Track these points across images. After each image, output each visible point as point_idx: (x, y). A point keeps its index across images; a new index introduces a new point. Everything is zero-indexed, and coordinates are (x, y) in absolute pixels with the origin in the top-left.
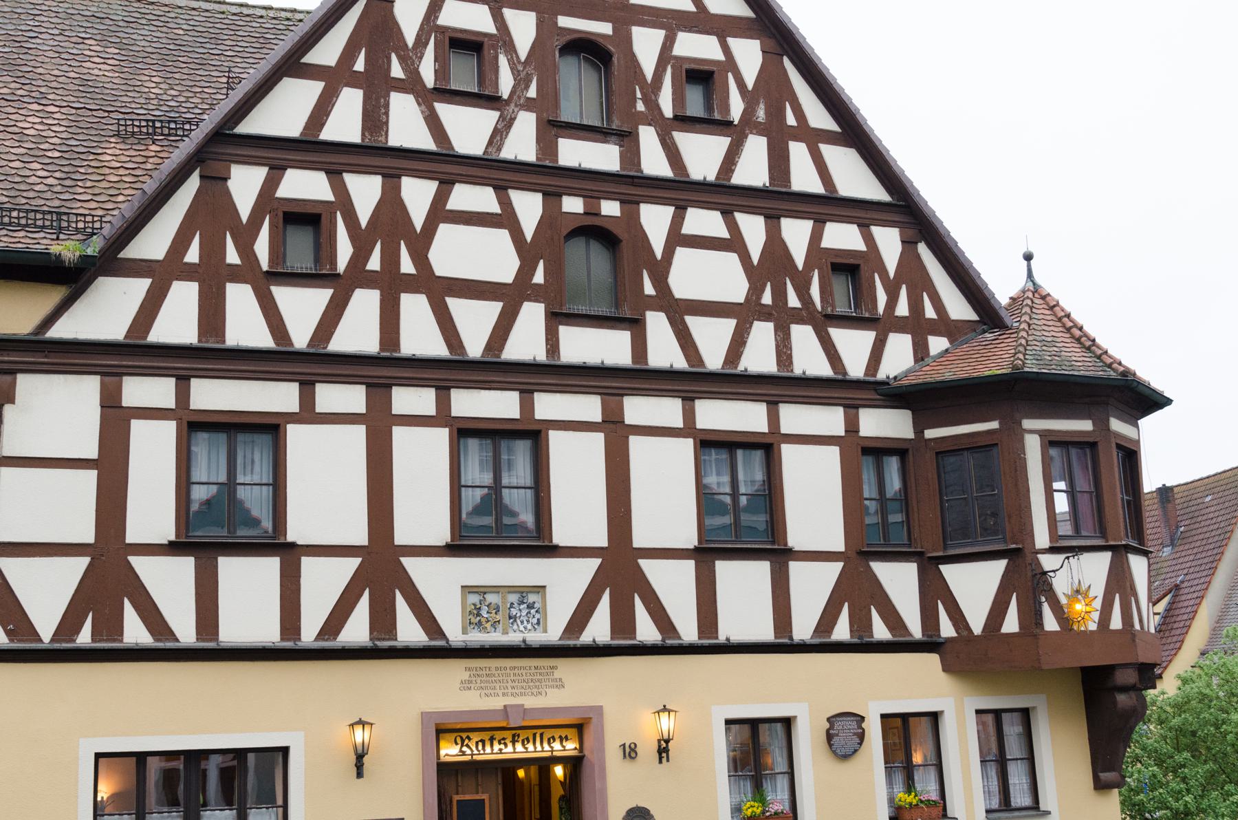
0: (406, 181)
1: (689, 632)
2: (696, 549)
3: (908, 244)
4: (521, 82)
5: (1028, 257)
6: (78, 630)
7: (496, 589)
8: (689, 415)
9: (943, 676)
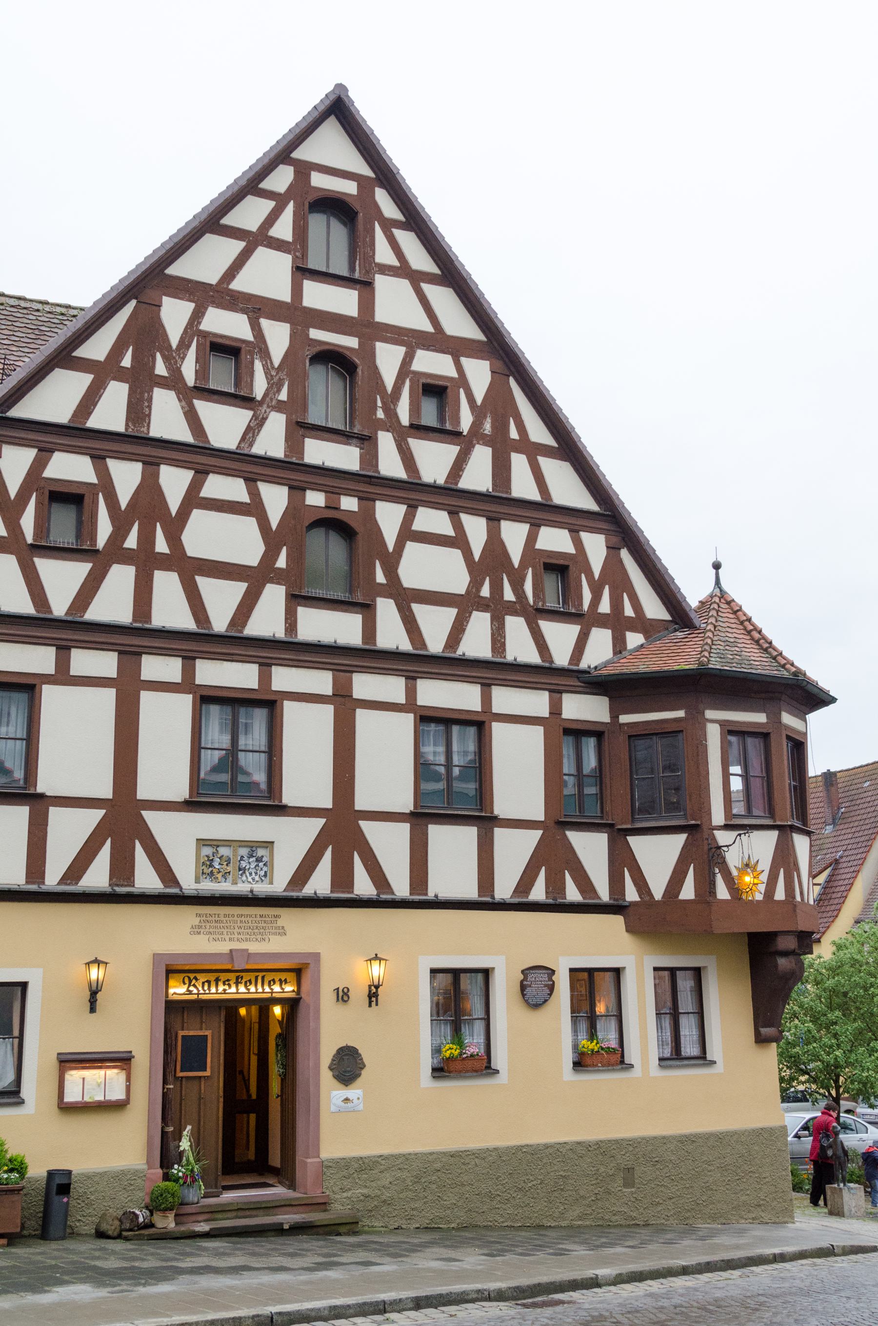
1: (401, 888)
2: (412, 814)
3: (612, 549)
4: (274, 386)
5: (717, 566)
7: (227, 843)
8: (411, 693)
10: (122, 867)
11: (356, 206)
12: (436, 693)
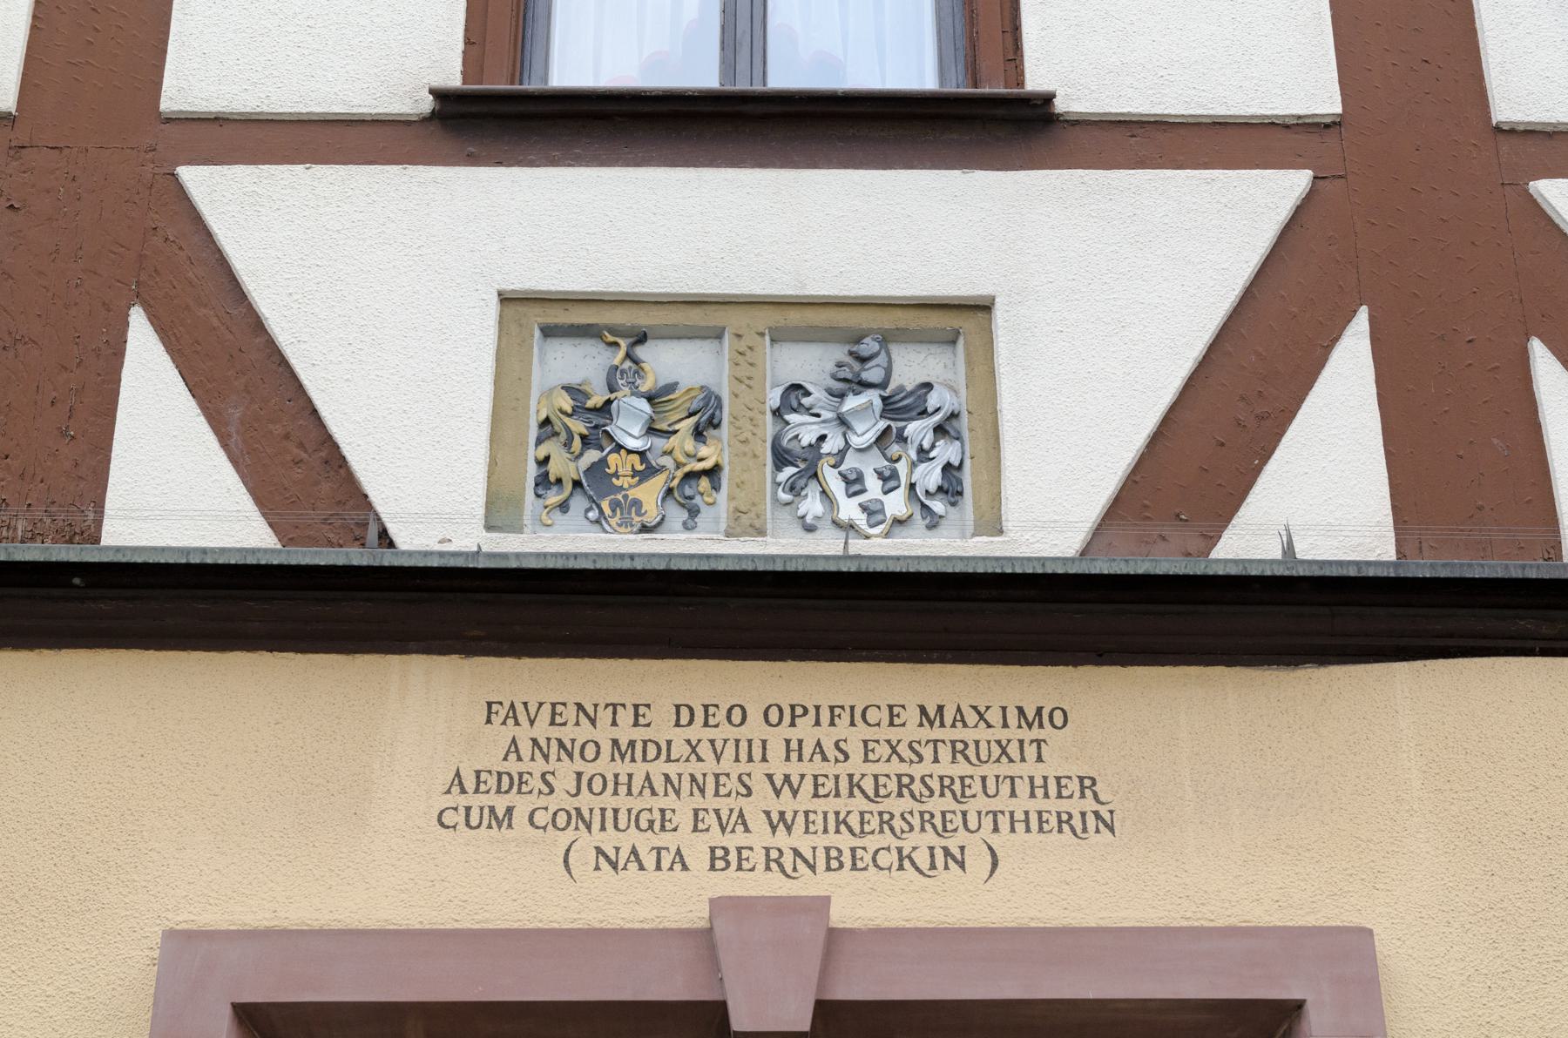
7: (700, 315)
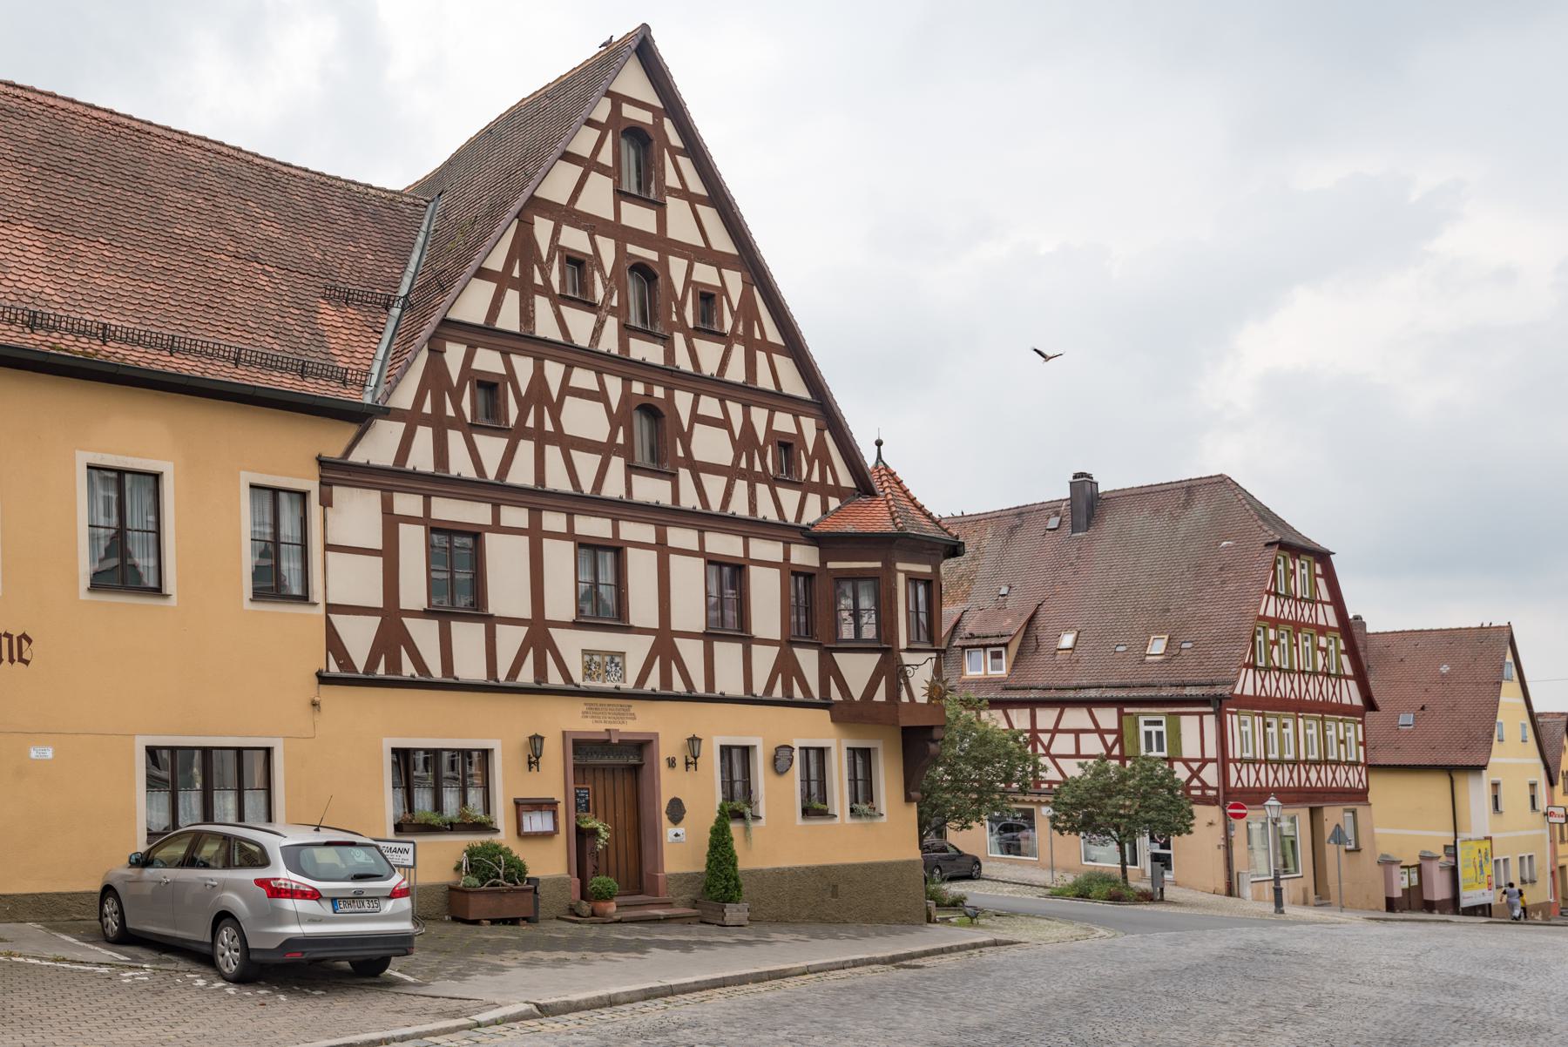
0: (547, 362)
1: (700, 689)
2: (705, 634)
3: (820, 430)
4: (608, 295)
5: (879, 443)
6: (377, 666)
7: (598, 652)
8: (570, 525)
9: (831, 726)
10: (666, 680)
11: (652, 135)
12: (447, 510)
